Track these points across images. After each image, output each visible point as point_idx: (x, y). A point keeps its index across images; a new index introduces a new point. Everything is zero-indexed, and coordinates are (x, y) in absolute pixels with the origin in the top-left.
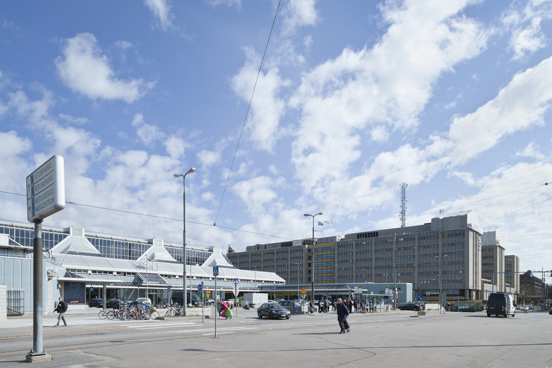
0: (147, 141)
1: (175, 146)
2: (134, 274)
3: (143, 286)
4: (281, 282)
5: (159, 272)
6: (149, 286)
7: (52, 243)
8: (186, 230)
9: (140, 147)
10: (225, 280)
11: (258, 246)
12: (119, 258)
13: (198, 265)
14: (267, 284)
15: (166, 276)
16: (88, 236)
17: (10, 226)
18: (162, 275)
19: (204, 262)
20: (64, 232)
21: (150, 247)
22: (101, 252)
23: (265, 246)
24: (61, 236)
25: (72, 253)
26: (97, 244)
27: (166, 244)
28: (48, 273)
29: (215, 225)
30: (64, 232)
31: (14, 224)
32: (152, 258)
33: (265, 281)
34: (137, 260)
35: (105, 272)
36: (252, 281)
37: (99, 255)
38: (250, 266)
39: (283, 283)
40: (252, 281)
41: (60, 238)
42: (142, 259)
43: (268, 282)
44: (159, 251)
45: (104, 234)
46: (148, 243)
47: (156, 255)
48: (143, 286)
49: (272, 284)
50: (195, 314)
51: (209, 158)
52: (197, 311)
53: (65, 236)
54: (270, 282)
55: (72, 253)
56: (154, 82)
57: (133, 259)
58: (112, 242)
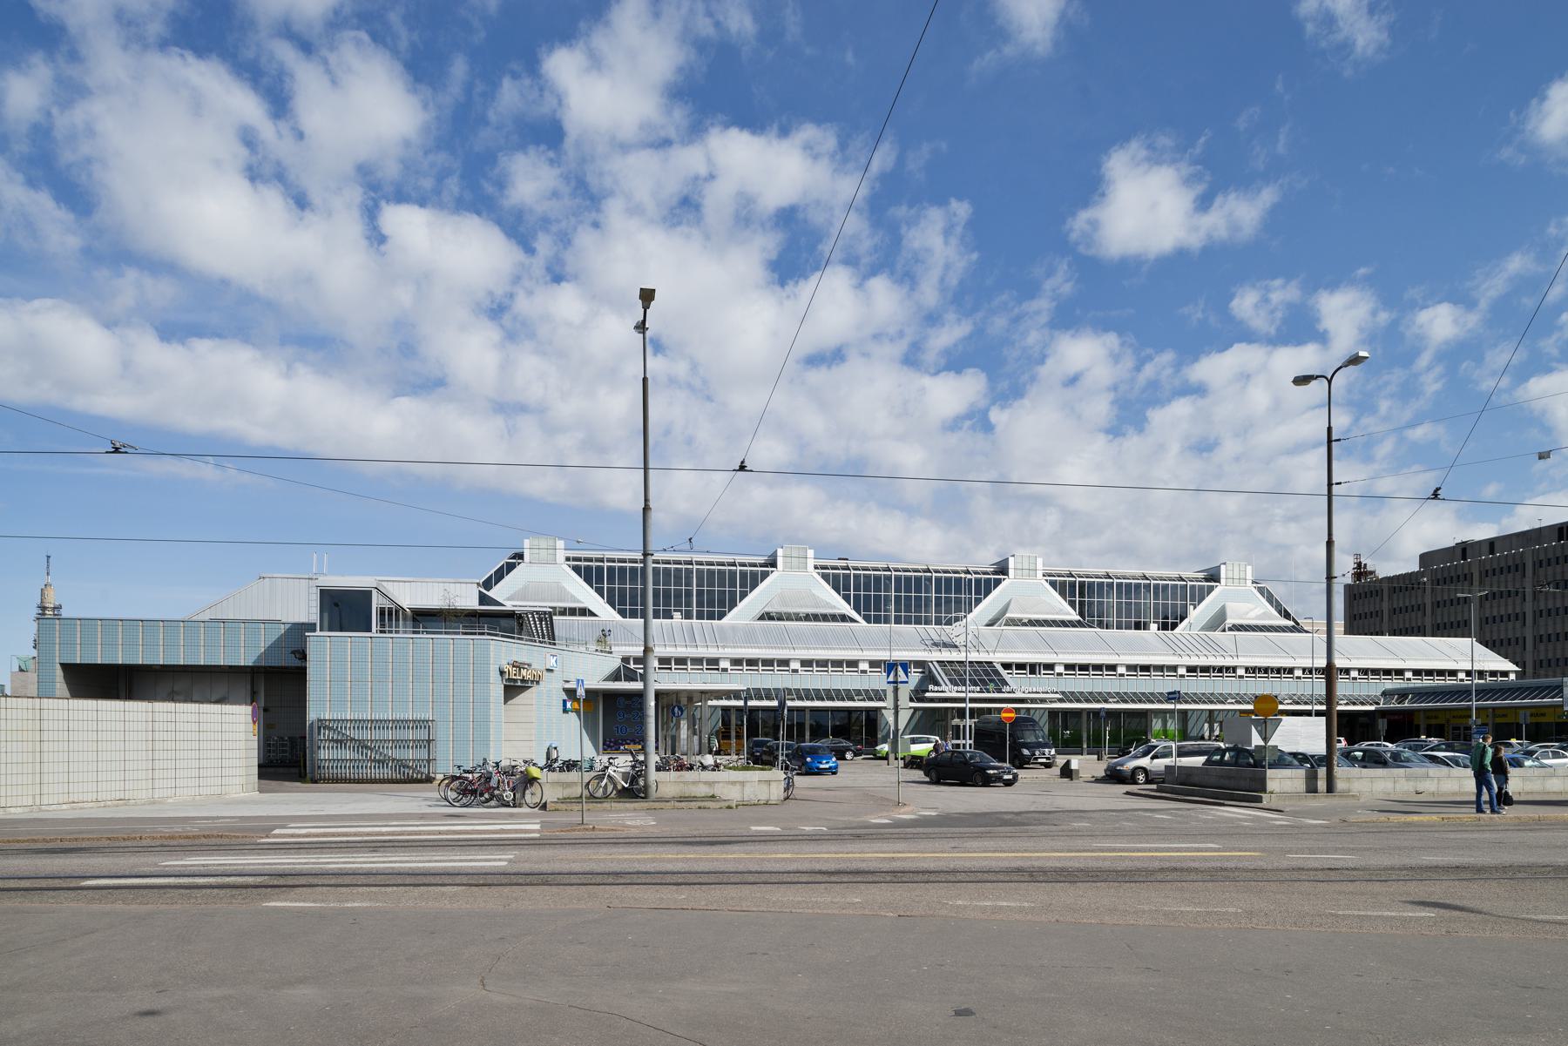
0: (1260, 323)
1: (1345, 315)
2: (920, 664)
3: (932, 700)
4: (1493, 673)
5: (998, 658)
6: (973, 700)
7: (733, 594)
8: (651, 504)
9: (1247, 336)
10: (1241, 672)
11: (1464, 549)
12: (908, 622)
13: (1154, 627)
14: (1427, 682)
15: (1021, 666)
16: (825, 568)
17: (598, 560)
18: (1007, 666)
19: (733, 605)
20: (995, 573)
21: (1211, 589)
22: (1081, 614)
23: (1491, 544)
24: (988, 581)
25: (1013, 622)
26: (600, 580)
27: (572, 554)
28: (502, 673)
29: (1435, 495)
30: (995, 573)
31: (851, 564)
32: (1217, 622)
33: (1417, 672)
34: (1177, 630)
35: (1098, 667)
36: (1354, 674)
37: (1079, 624)
38: (1428, 621)
39: (1505, 674)
40: (1354, 674)
41: (985, 587)
42: (743, 613)
43: (1429, 673)
44: (798, 583)
45: (1090, 567)
46: (1207, 580)
47: (1229, 613)
48: (932, 700)
49: (1450, 681)
50: (702, 790)
51: (1440, 323)
52: (710, 784)
53: (998, 582)
54: (1441, 673)
55: (1013, 622)
56: (1268, 196)
57: (711, 616)
58: (1110, 585)
